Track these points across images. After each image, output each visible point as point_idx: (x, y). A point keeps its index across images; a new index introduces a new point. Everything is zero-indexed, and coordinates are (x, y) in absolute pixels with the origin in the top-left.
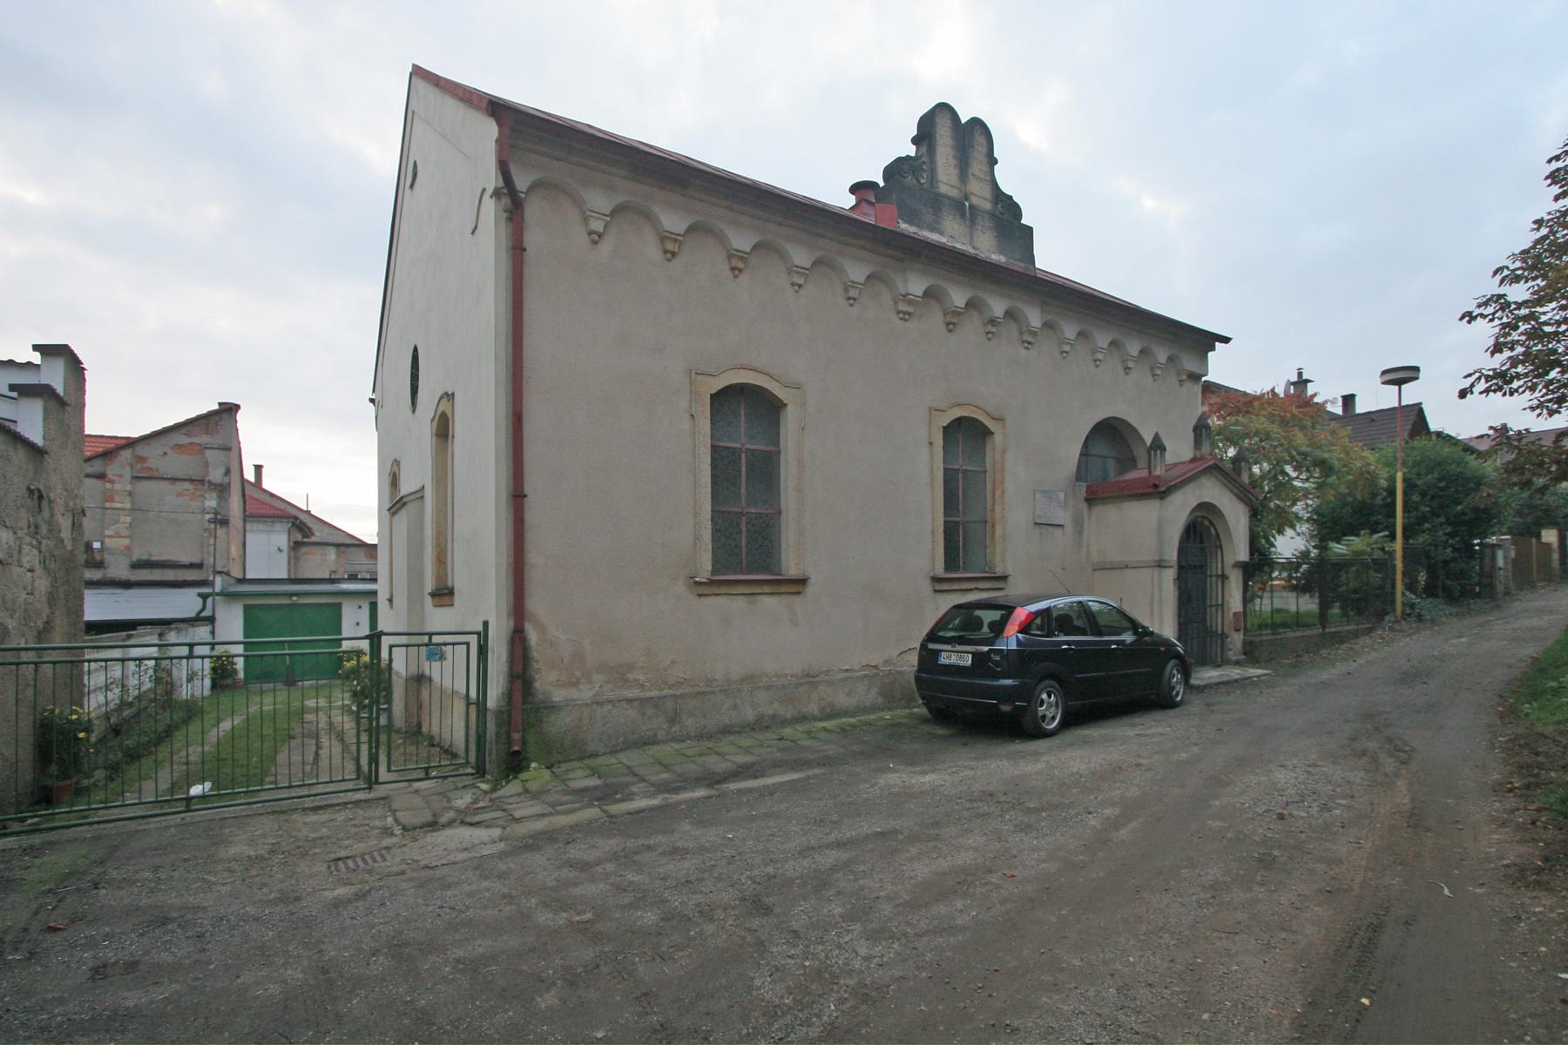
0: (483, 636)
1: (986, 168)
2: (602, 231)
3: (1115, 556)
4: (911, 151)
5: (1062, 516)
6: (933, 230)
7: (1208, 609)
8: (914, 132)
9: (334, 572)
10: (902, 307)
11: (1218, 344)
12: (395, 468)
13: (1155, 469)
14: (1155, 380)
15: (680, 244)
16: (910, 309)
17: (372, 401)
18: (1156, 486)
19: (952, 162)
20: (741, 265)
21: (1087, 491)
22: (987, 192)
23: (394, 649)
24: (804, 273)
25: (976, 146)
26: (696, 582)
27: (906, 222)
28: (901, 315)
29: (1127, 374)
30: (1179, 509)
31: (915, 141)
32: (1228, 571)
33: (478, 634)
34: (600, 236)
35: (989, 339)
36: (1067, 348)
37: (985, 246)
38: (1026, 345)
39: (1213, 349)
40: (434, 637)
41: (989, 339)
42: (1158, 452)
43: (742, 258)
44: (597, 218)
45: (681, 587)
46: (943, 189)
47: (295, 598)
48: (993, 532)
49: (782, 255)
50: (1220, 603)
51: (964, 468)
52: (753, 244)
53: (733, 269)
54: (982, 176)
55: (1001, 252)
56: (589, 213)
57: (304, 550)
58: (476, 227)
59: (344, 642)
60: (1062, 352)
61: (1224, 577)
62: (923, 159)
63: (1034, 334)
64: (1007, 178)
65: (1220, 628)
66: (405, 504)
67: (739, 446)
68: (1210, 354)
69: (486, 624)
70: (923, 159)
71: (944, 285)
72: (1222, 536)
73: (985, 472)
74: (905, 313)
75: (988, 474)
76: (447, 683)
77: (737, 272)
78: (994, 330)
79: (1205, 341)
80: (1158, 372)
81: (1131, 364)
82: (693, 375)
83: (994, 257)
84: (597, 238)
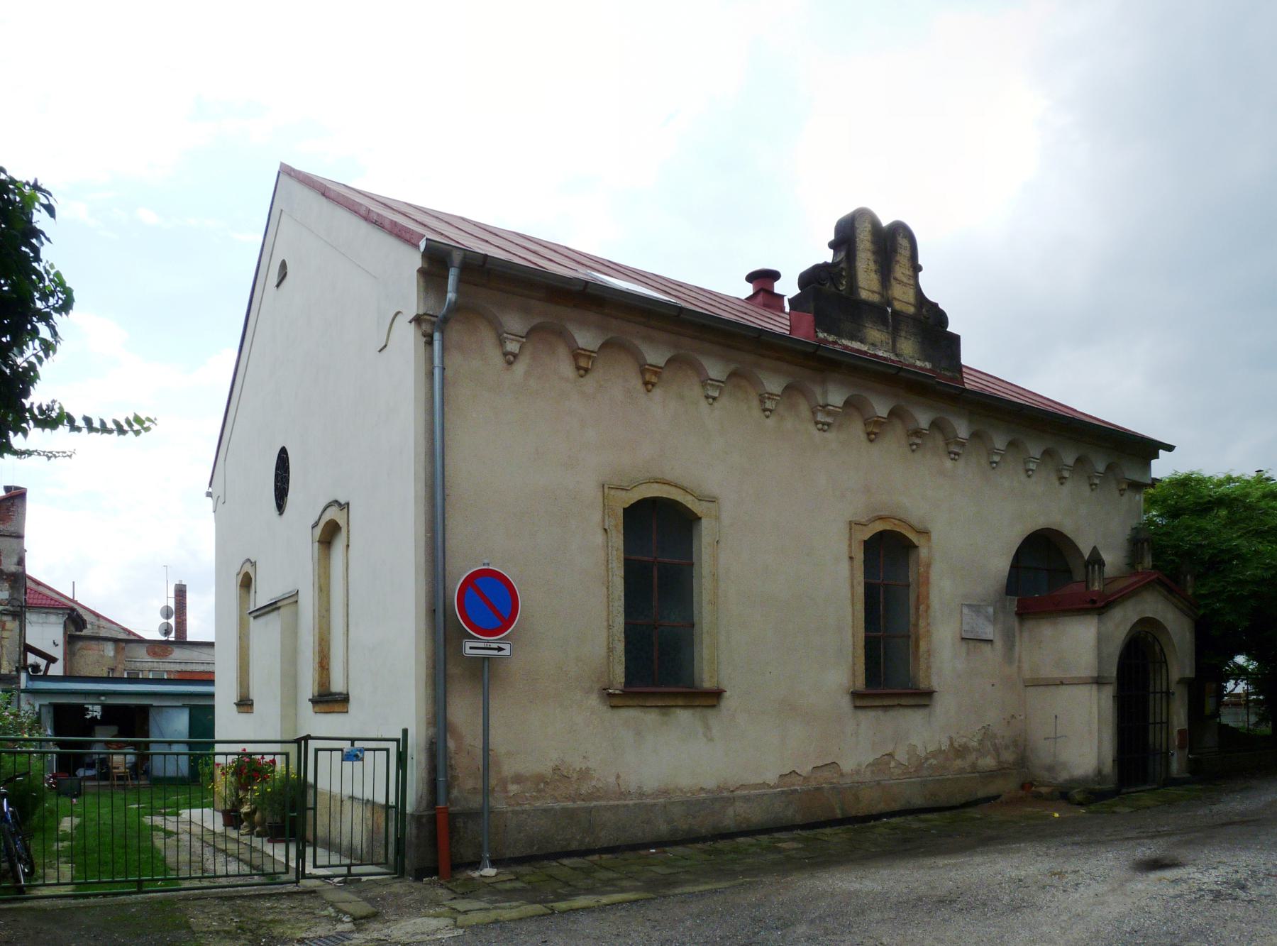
0: (402, 743)
1: (909, 273)
2: (517, 352)
3: (1049, 671)
4: (827, 256)
5: (989, 631)
6: (852, 338)
7: (1151, 727)
8: (832, 237)
9: (113, 670)
10: (820, 417)
11: (1161, 452)
12: (248, 568)
13: (1093, 585)
14: (1092, 490)
15: (594, 360)
16: (829, 420)
17: (209, 495)
18: (1094, 602)
19: (873, 266)
20: (654, 379)
21: (1018, 606)
22: (910, 296)
23: (319, 752)
24: (718, 386)
25: (900, 250)
26: (609, 694)
27: (824, 331)
28: (820, 426)
29: (1062, 484)
30: (1121, 621)
31: (832, 245)
32: (1173, 688)
33: (397, 741)
34: (515, 356)
35: (913, 451)
36: (996, 458)
37: (908, 351)
38: (953, 456)
39: (1157, 457)
40: (356, 742)
41: (913, 451)
42: (1096, 567)
43: (655, 373)
44: (513, 340)
45: (594, 701)
46: (864, 295)
47: (103, 698)
48: (917, 646)
49: (698, 369)
50: (1164, 720)
51: (885, 582)
52: (667, 359)
53: (646, 383)
54: (905, 280)
55: (926, 358)
56: (505, 335)
57: (80, 644)
58: (385, 346)
59: (217, 746)
60: (991, 463)
61: (1168, 694)
62: (842, 265)
63: (962, 445)
64: (932, 286)
65: (1164, 746)
66: (278, 608)
67: (651, 559)
68: (1153, 462)
69: (405, 732)
70: (842, 265)
71: (863, 394)
72: (1165, 650)
73: (908, 586)
74: (823, 424)
75: (911, 587)
76: (336, 789)
77: (650, 387)
78: (918, 441)
79: (1148, 449)
80: (1097, 481)
81: (1066, 474)
82: (606, 490)
83: (918, 363)
84: (512, 358)
